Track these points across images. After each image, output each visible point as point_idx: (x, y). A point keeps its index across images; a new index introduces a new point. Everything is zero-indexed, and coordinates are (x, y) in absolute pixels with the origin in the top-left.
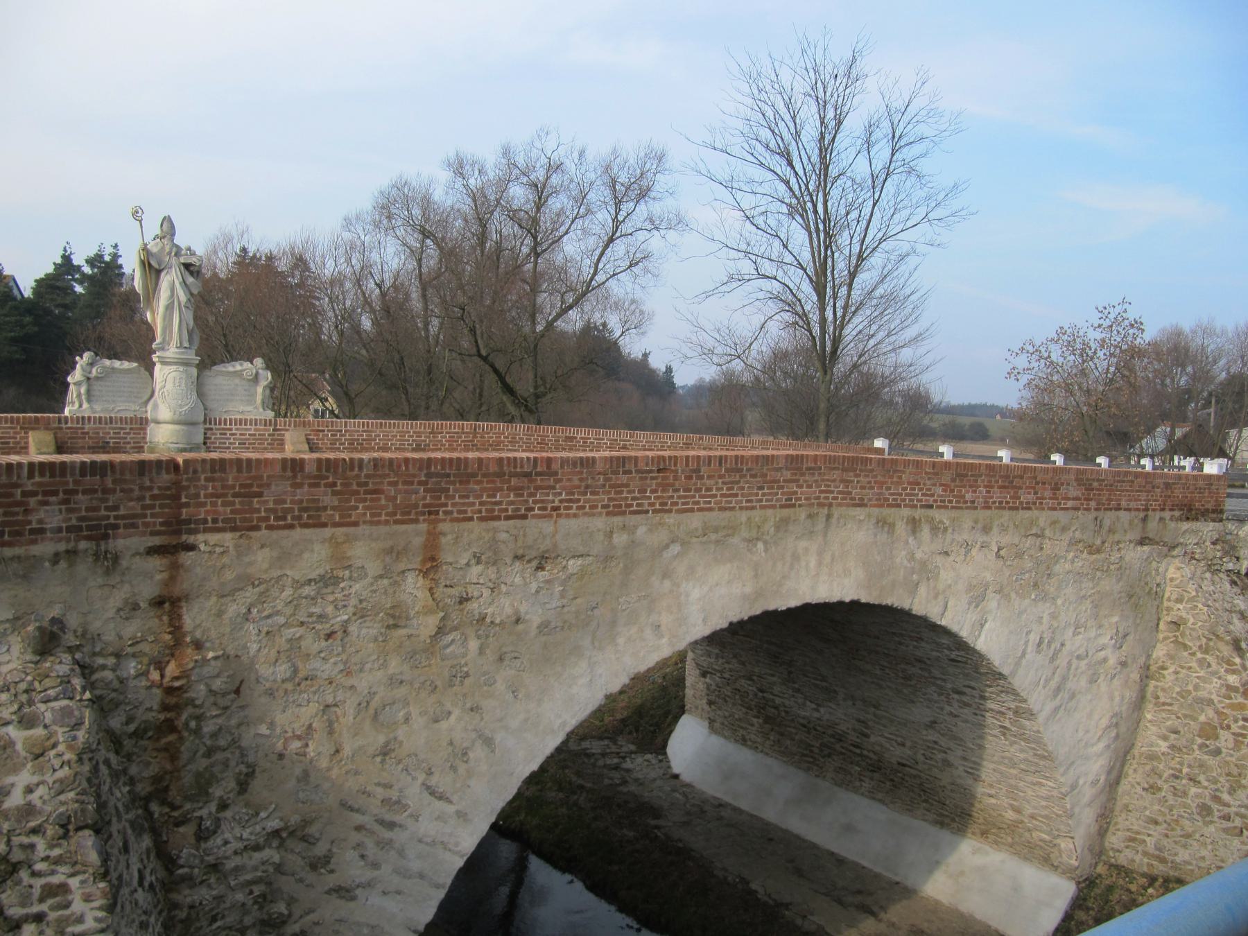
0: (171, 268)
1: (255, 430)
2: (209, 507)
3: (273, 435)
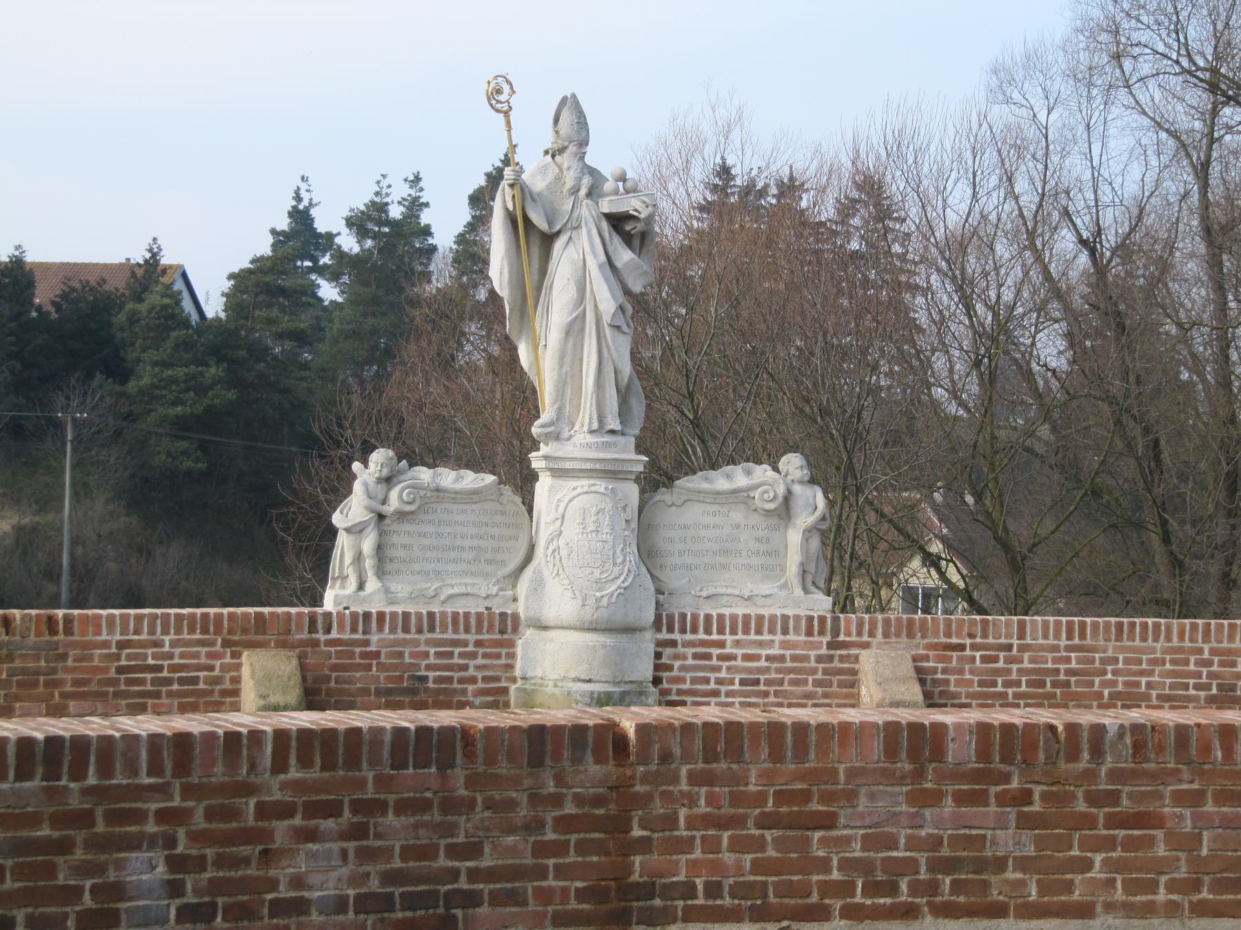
0: (578, 227)
1: (785, 645)
2: (697, 854)
3: (830, 658)
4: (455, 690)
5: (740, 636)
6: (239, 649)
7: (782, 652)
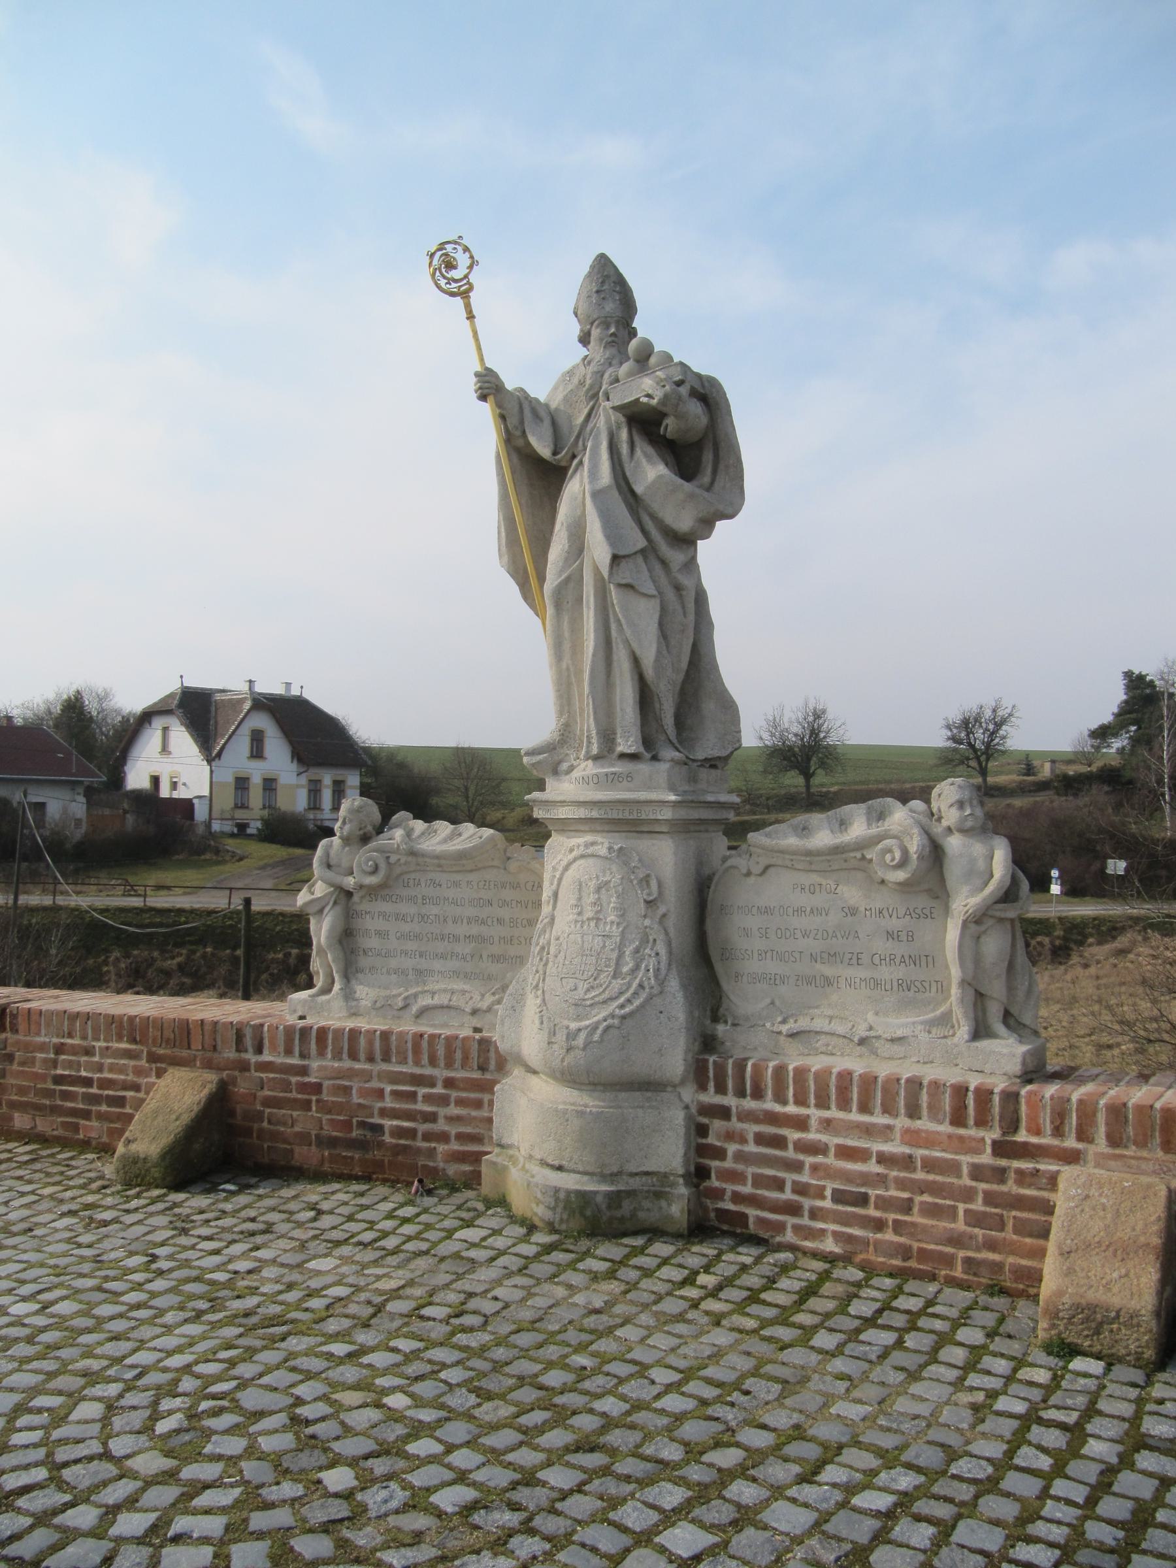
3: (1000, 1175)
4: (419, 1151)
5: (834, 1113)
6: (163, 1065)
7: (907, 1150)
